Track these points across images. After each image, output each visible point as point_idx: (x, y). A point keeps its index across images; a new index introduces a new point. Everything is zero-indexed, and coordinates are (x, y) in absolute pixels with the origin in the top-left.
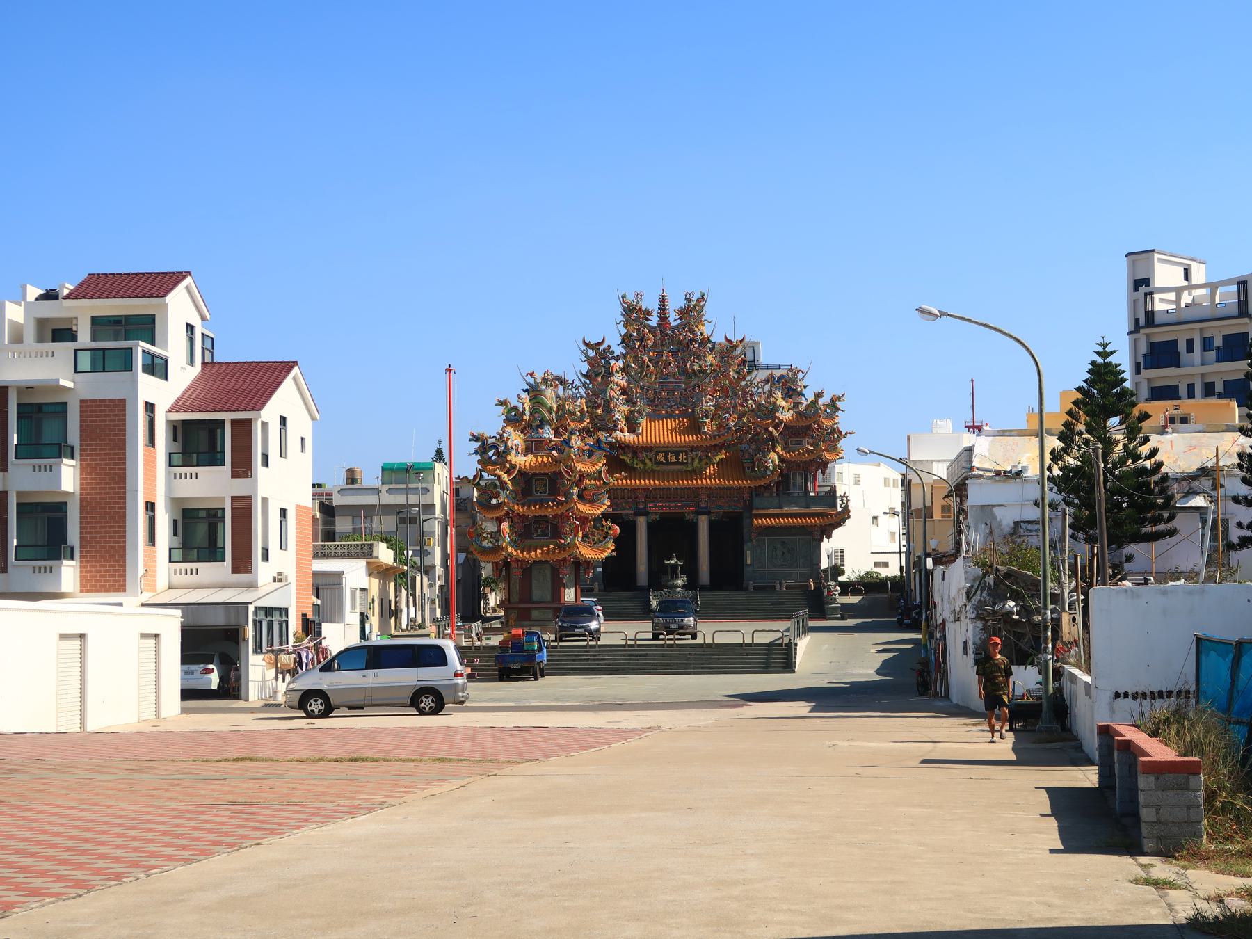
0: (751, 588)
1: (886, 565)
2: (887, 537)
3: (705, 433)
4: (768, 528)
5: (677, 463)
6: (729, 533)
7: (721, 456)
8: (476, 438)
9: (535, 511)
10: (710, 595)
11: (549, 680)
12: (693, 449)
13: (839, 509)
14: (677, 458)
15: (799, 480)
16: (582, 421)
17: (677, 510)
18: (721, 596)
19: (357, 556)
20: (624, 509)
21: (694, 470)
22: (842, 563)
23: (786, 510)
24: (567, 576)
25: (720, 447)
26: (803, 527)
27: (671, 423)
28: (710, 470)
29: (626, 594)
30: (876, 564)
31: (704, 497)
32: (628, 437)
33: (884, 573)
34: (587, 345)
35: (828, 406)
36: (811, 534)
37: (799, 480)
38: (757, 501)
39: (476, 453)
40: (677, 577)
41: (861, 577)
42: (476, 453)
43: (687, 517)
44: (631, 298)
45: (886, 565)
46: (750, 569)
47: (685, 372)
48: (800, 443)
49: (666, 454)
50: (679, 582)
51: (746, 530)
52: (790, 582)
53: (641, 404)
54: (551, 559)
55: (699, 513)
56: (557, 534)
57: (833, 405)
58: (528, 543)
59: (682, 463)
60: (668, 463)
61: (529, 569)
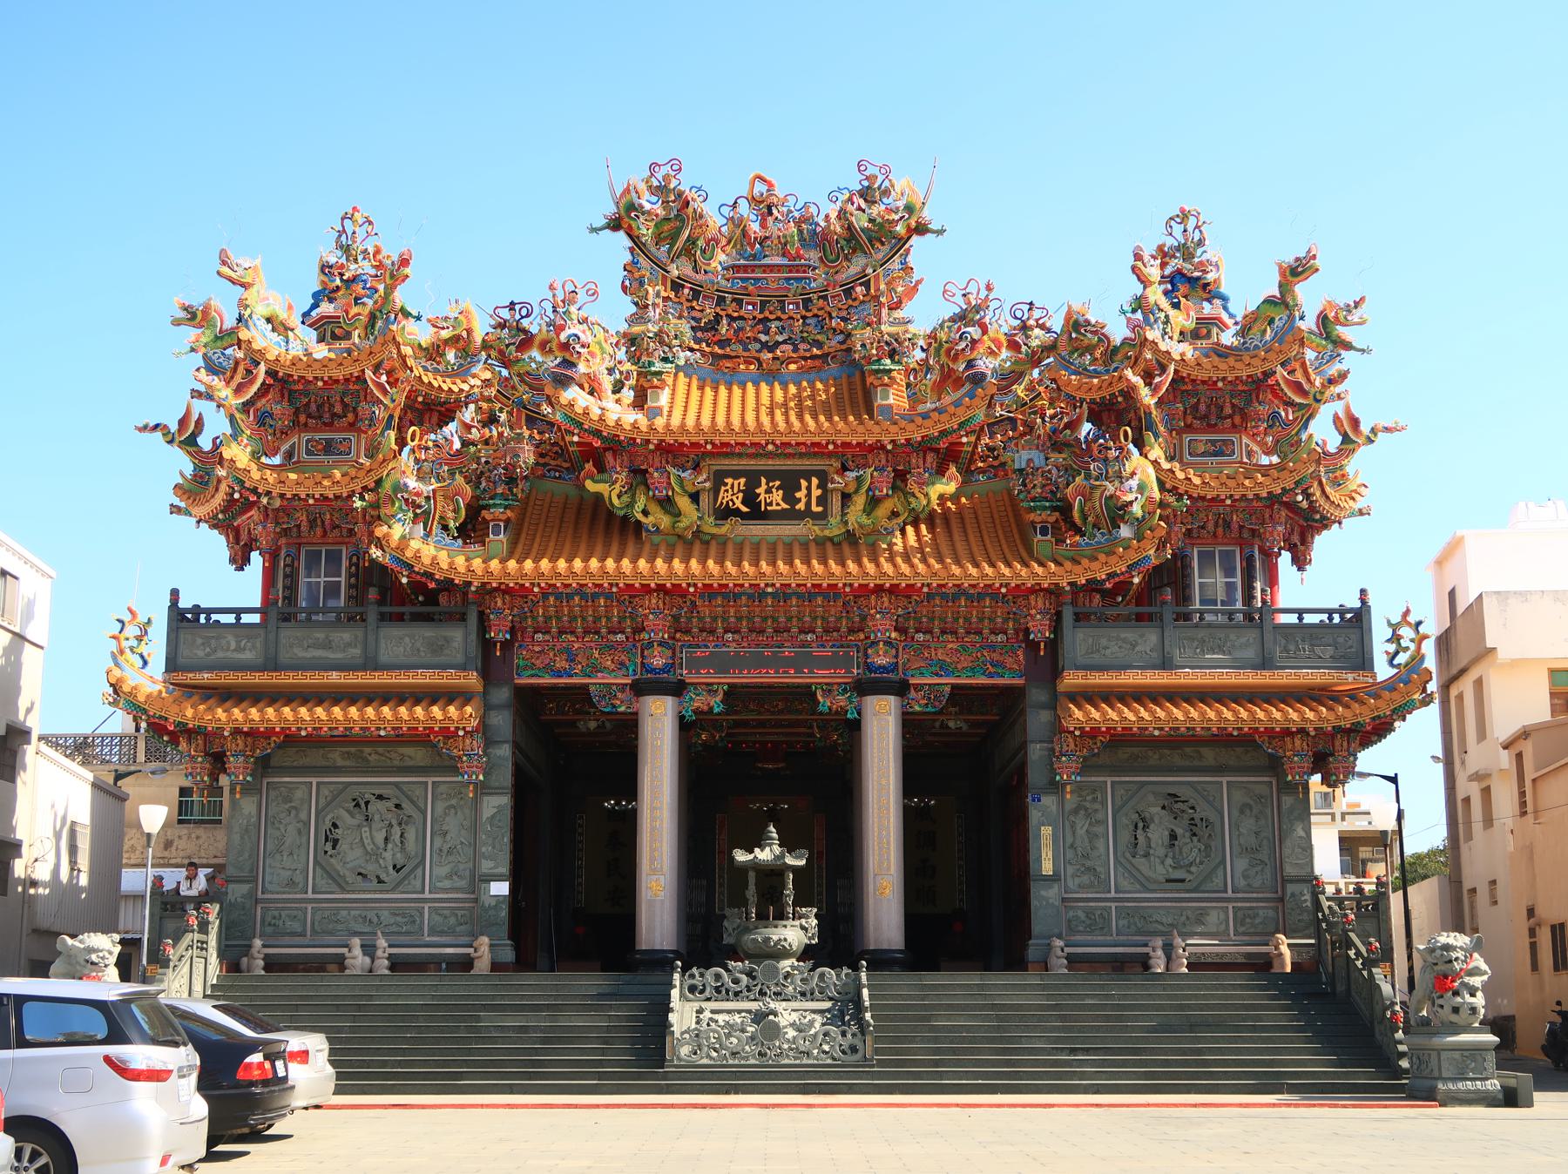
0: (1059, 965)
4: (1120, 739)
5: (791, 515)
6: (974, 776)
10: (906, 984)
12: (850, 456)
14: (790, 498)
18: (958, 990)
20: (596, 669)
21: (851, 537)
23: (1187, 677)
25: (945, 455)
29: (589, 982)
31: (882, 625)
32: (617, 412)
36: (1275, 766)
40: (781, 916)
41: (1023, 712)
43: (824, 703)
49: (753, 482)
51: (1036, 752)
60: (756, 512)
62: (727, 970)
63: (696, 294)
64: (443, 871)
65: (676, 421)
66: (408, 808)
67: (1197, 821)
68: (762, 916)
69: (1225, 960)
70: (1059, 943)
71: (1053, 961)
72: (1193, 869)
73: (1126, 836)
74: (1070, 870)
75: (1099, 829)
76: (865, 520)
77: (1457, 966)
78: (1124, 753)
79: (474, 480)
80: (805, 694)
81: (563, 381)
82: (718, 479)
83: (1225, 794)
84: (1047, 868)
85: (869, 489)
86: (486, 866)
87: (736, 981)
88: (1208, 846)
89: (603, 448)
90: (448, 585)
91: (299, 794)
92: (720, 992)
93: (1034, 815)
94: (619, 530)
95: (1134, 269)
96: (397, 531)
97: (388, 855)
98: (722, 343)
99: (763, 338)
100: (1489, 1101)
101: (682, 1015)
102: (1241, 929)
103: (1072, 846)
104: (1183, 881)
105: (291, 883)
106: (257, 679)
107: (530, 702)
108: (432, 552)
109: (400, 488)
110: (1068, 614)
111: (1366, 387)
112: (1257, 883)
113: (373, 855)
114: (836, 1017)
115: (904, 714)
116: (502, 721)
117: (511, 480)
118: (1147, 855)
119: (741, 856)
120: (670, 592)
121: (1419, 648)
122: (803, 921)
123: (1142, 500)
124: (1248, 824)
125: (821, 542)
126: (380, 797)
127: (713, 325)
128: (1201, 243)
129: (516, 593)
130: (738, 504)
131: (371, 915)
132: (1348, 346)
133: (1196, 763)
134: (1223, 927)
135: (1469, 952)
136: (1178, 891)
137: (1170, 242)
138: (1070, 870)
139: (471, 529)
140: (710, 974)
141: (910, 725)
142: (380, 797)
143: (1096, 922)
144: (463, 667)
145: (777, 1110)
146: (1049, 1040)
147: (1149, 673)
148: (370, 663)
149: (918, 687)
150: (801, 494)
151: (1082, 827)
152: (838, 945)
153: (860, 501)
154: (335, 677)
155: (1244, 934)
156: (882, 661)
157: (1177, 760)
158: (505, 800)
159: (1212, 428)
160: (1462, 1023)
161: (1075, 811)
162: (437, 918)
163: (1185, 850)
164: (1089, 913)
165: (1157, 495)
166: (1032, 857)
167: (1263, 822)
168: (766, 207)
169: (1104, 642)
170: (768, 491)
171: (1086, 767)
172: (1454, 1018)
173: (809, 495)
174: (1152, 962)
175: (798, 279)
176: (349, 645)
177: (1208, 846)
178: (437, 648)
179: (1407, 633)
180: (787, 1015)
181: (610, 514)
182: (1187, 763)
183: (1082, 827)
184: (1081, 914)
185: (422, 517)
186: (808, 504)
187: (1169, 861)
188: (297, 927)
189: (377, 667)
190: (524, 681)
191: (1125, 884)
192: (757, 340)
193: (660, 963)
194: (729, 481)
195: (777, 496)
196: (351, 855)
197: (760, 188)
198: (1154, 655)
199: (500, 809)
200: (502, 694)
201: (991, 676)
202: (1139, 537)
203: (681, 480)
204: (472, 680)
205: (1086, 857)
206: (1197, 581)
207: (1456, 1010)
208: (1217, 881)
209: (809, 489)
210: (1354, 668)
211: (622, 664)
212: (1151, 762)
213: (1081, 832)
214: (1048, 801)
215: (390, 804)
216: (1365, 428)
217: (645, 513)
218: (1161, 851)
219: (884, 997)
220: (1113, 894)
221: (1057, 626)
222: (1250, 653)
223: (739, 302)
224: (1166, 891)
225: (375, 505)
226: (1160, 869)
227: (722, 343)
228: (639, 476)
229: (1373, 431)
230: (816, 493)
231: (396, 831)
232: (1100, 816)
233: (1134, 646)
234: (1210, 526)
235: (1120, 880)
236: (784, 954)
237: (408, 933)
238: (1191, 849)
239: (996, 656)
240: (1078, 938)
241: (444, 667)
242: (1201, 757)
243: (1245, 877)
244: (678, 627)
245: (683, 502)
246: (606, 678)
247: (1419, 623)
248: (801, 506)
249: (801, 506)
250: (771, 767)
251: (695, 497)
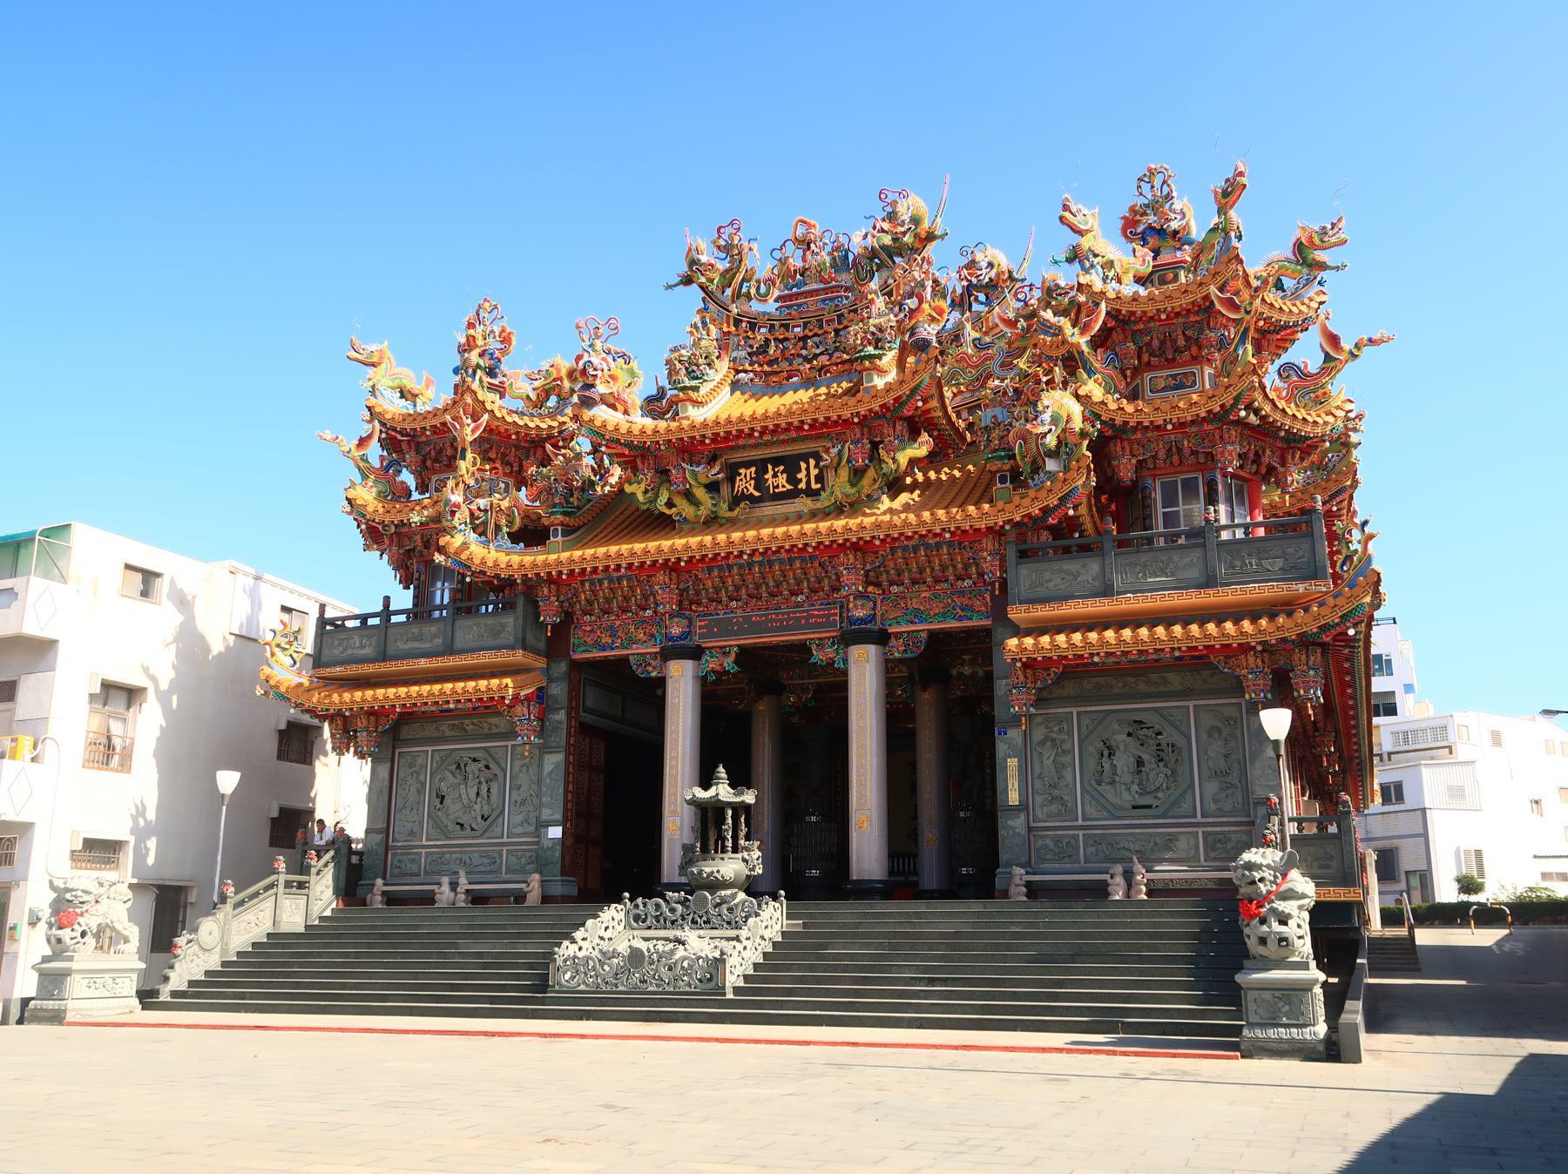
14: (793, 480)
20: (632, 642)
22: (1482, 874)
31: (852, 582)
38: (1025, 577)
43: (818, 656)
52: (1168, 871)
60: (768, 496)
62: (666, 901)
63: (752, 326)
64: (518, 819)
66: (495, 769)
67: (1164, 746)
69: (1195, 886)
70: (1018, 871)
71: (1013, 890)
72: (1160, 795)
73: (1092, 765)
74: (1039, 800)
75: (1066, 759)
76: (849, 490)
77: (1263, 888)
78: (1088, 684)
80: (803, 648)
82: (732, 472)
83: (1192, 718)
84: (1014, 798)
85: (849, 461)
86: (546, 814)
87: (673, 910)
88: (1174, 772)
91: (420, 761)
93: (1001, 748)
95: (1061, 219)
97: (477, 807)
98: (770, 363)
99: (804, 352)
100: (1308, 1053)
102: (1213, 855)
103: (1040, 777)
104: (1149, 807)
105: (412, 833)
106: (369, 669)
111: (1342, 303)
112: (1228, 807)
113: (468, 808)
115: (887, 661)
118: (1112, 783)
120: (671, 566)
121: (1365, 548)
122: (745, 854)
123: (1056, 431)
124: (1217, 747)
126: (475, 760)
128: (1169, 197)
130: (752, 490)
131: (465, 858)
132: (1322, 266)
133: (1162, 688)
134: (1192, 853)
136: (1146, 817)
137: (1141, 201)
138: (1039, 800)
140: (651, 903)
141: (889, 667)
142: (475, 760)
143: (1065, 851)
144: (512, 648)
145: (497, 1038)
146: (918, 969)
147: (1090, 602)
148: (450, 650)
149: (898, 635)
150: (802, 475)
151: (1049, 756)
154: (423, 663)
155: (1215, 859)
157: (1142, 687)
158: (560, 757)
159: (1171, 363)
160: (1273, 957)
161: (1042, 743)
162: (513, 859)
163: (1151, 775)
164: (1057, 840)
166: (999, 788)
167: (1233, 744)
168: (805, 244)
169: (1047, 575)
170: (775, 476)
172: (1261, 950)
173: (808, 475)
174: (1110, 889)
175: (831, 299)
176: (434, 636)
177: (1174, 772)
178: (496, 633)
182: (1153, 689)
183: (1049, 756)
184: (1048, 842)
186: (808, 482)
187: (1135, 788)
188: (415, 868)
190: (578, 656)
191: (1091, 811)
192: (799, 355)
194: (742, 471)
195: (782, 479)
196: (454, 808)
197: (801, 231)
198: (1097, 583)
199: (557, 765)
200: (562, 667)
201: (960, 619)
203: (694, 474)
205: (1053, 786)
206: (1160, 511)
207: (1263, 941)
208: (1186, 806)
209: (808, 469)
210: (1304, 579)
211: (652, 636)
212: (1116, 690)
213: (1048, 762)
215: (481, 765)
216: (1347, 345)
217: (670, 504)
218: (1127, 778)
219: (814, 925)
220: (1080, 822)
222: (1194, 573)
223: (786, 327)
224: (1133, 818)
226: (1126, 795)
229: (1357, 346)
230: (814, 472)
231: (484, 788)
232: (1067, 746)
233: (1076, 577)
234: (1162, 454)
235: (1087, 807)
237: (490, 872)
238: (1156, 775)
239: (966, 601)
240: (1046, 866)
241: (499, 648)
242: (1166, 682)
243: (1216, 801)
245: (700, 493)
246: (640, 649)
247: (1365, 523)
248: (802, 486)
249: (802, 486)
250: (776, 717)
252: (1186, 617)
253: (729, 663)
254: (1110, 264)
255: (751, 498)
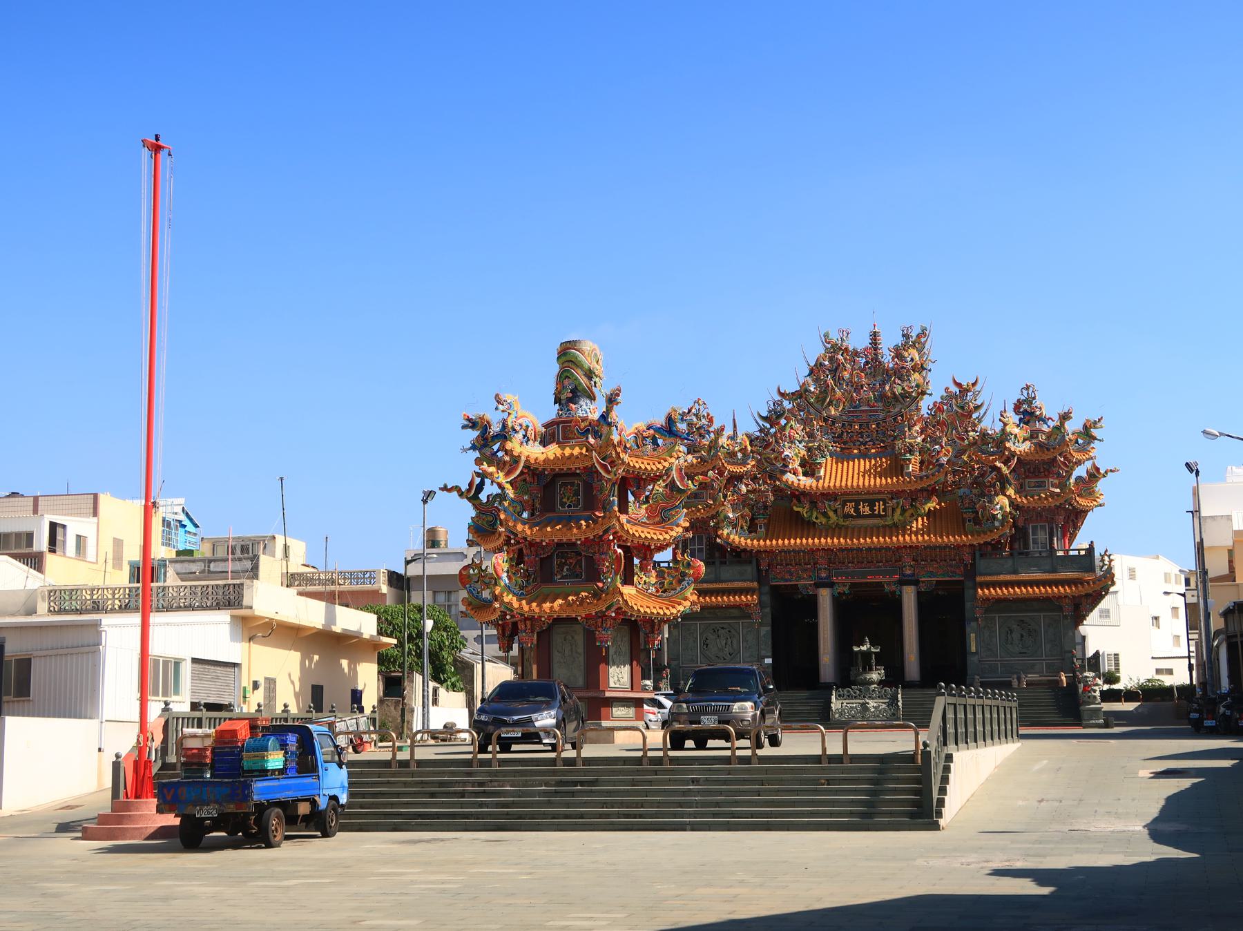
1: (1170, 672)
2: (1170, 640)
3: (909, 474)
4: (999, 601)
6: (946, 611)
7: (932, 505)
8: (472, 424)
9: (552, 533)
11: (348, 846)
12: (895, 494)
13: (1099, 573)
14: (872, 509)
15: (1042, 536)
16: (743, 463)
17: (870, 579)
19: (218, 606)
20: (800, 578)
22: (1117, 670)
23: (1023, 576)
24: (610, 640)
25: (930, 492)
26: (1047, 600)
27: (864, 464)
28: (918, 524)
29: (804, 694)
30: (1158, 671)
31: (907, 560)
32: (806, 482)
33: (1168, 681)
34: (782, 395)
35: (1079, 434)
37: (1042, 536)
38: (981, 564)
39: (474, 447)
40: (871, 669)
42: (474, 447)
43: (887, 588)
44: (834, 337)
45: (1170, 672)
46: (975, 659)
47: (882, 397)
48: (1041, 485)
49: (857, 504)
50: (875, 676)
51: (968, 605)
52: (1033, 677)
53: (824, 440)
54: (580, 613)
55: (904, 582)
56: (594, 574)
57: (1087, 433)
58: (546, 588)
59: (879, 516)
60: (859, 515)
61: (547, 631)
65: (826, 485)
68: (864, 669)
79: (751, 510)
81: (784, 473)
84: (973, 649)
86: (763, 653)
89: (799, 495)
90: (745, 550)
92: (850, 697)
93: (968, 629)
94: (804, 526)
96: (726, 532)
98: (845, 443)
101: (836, 704)
107: (775, 589)
108: (737, 539)
109: (727, 517)
110: (977, 554)
111: (1101, 455)
114: (889, 705)
116: (766, 599)
117: (766, 507)
119: (856, 649)
125: (884, 527)
127: (841, 436)
129: (770, 552)
132: (1095, 438)
135: (1094, 678)
139: (752, 529)
152: (895, 678)
153: (898, 511)
156: (908, 572)
158: (769, 628)
165: (1008, 509)
171: (987, 611)
179: (1106, 558)
180: (872, 704)
181: (803, 518)
185: (735, 527)
189: (720, 582)
193: (828, 688)
195: (867, 509)
200: (766, 589)
202: (1003, 525)
204: (755, 585)
214: (974, 624)
216: (1102, 471)
221: (974, 559)
225: (717, 523)
227: (845, 443)
228: (814, 505)
236: (873, 683)
241: (744, 581)
244: (830, 562)
245: (831, 514)
250: (867, 613)
251: (835, 511)
252: (1044, 583)
253: (846, 590)
254: (1016, 436)
255: (852, 516)
